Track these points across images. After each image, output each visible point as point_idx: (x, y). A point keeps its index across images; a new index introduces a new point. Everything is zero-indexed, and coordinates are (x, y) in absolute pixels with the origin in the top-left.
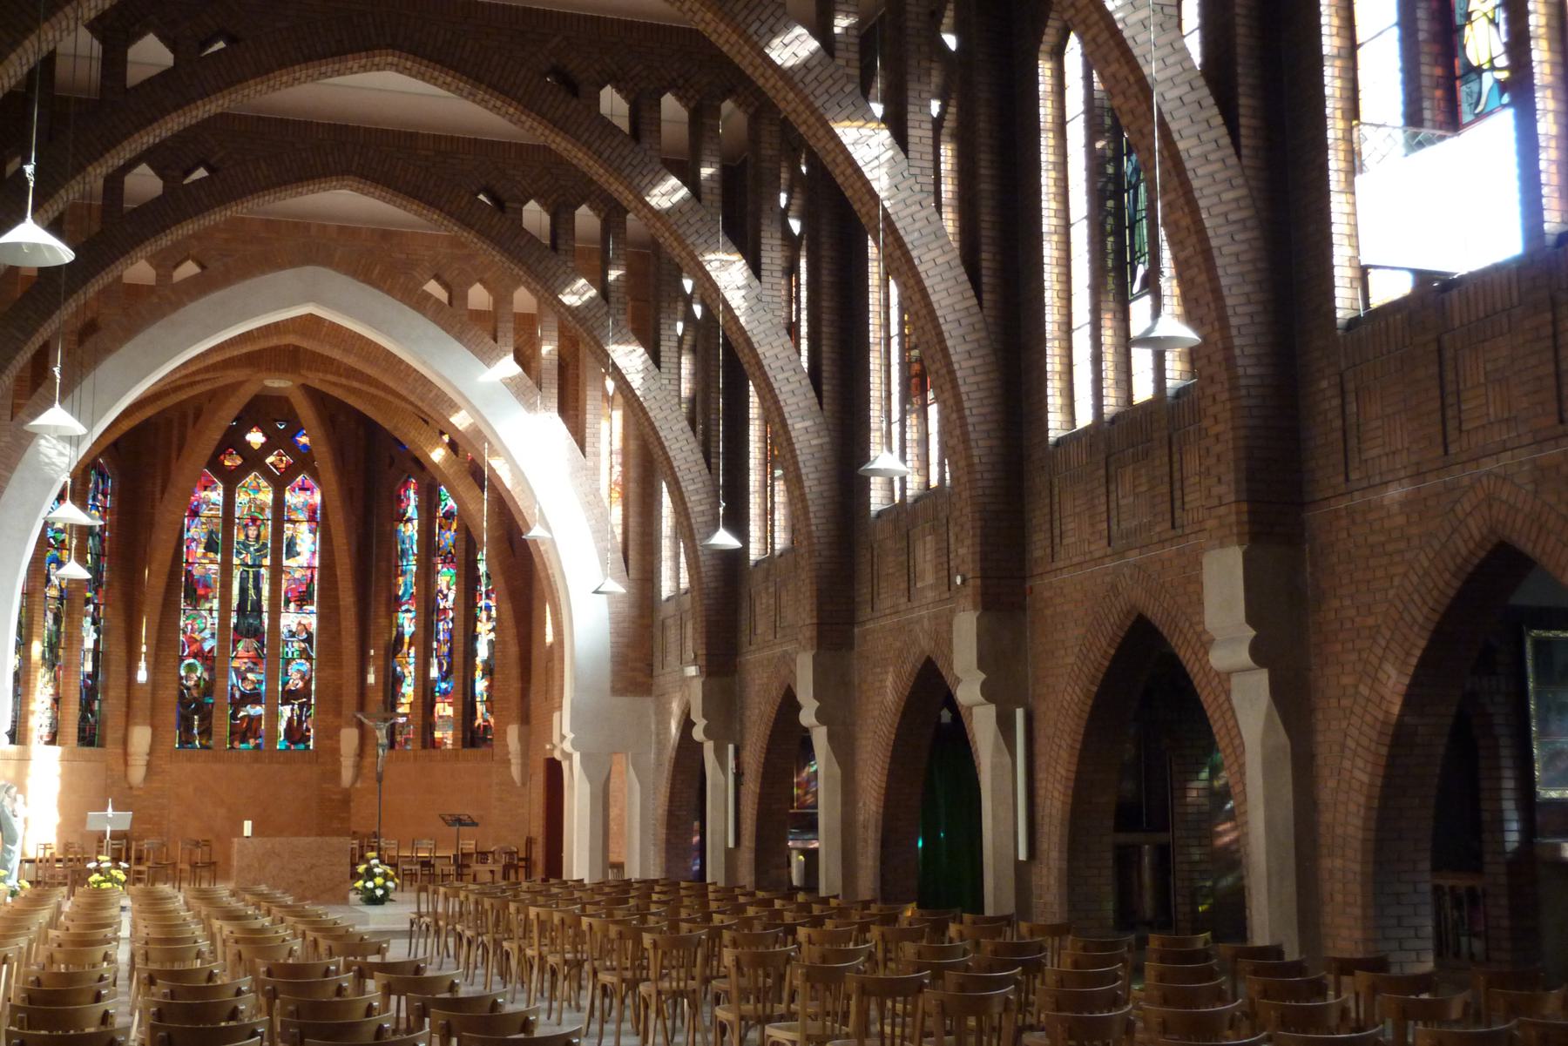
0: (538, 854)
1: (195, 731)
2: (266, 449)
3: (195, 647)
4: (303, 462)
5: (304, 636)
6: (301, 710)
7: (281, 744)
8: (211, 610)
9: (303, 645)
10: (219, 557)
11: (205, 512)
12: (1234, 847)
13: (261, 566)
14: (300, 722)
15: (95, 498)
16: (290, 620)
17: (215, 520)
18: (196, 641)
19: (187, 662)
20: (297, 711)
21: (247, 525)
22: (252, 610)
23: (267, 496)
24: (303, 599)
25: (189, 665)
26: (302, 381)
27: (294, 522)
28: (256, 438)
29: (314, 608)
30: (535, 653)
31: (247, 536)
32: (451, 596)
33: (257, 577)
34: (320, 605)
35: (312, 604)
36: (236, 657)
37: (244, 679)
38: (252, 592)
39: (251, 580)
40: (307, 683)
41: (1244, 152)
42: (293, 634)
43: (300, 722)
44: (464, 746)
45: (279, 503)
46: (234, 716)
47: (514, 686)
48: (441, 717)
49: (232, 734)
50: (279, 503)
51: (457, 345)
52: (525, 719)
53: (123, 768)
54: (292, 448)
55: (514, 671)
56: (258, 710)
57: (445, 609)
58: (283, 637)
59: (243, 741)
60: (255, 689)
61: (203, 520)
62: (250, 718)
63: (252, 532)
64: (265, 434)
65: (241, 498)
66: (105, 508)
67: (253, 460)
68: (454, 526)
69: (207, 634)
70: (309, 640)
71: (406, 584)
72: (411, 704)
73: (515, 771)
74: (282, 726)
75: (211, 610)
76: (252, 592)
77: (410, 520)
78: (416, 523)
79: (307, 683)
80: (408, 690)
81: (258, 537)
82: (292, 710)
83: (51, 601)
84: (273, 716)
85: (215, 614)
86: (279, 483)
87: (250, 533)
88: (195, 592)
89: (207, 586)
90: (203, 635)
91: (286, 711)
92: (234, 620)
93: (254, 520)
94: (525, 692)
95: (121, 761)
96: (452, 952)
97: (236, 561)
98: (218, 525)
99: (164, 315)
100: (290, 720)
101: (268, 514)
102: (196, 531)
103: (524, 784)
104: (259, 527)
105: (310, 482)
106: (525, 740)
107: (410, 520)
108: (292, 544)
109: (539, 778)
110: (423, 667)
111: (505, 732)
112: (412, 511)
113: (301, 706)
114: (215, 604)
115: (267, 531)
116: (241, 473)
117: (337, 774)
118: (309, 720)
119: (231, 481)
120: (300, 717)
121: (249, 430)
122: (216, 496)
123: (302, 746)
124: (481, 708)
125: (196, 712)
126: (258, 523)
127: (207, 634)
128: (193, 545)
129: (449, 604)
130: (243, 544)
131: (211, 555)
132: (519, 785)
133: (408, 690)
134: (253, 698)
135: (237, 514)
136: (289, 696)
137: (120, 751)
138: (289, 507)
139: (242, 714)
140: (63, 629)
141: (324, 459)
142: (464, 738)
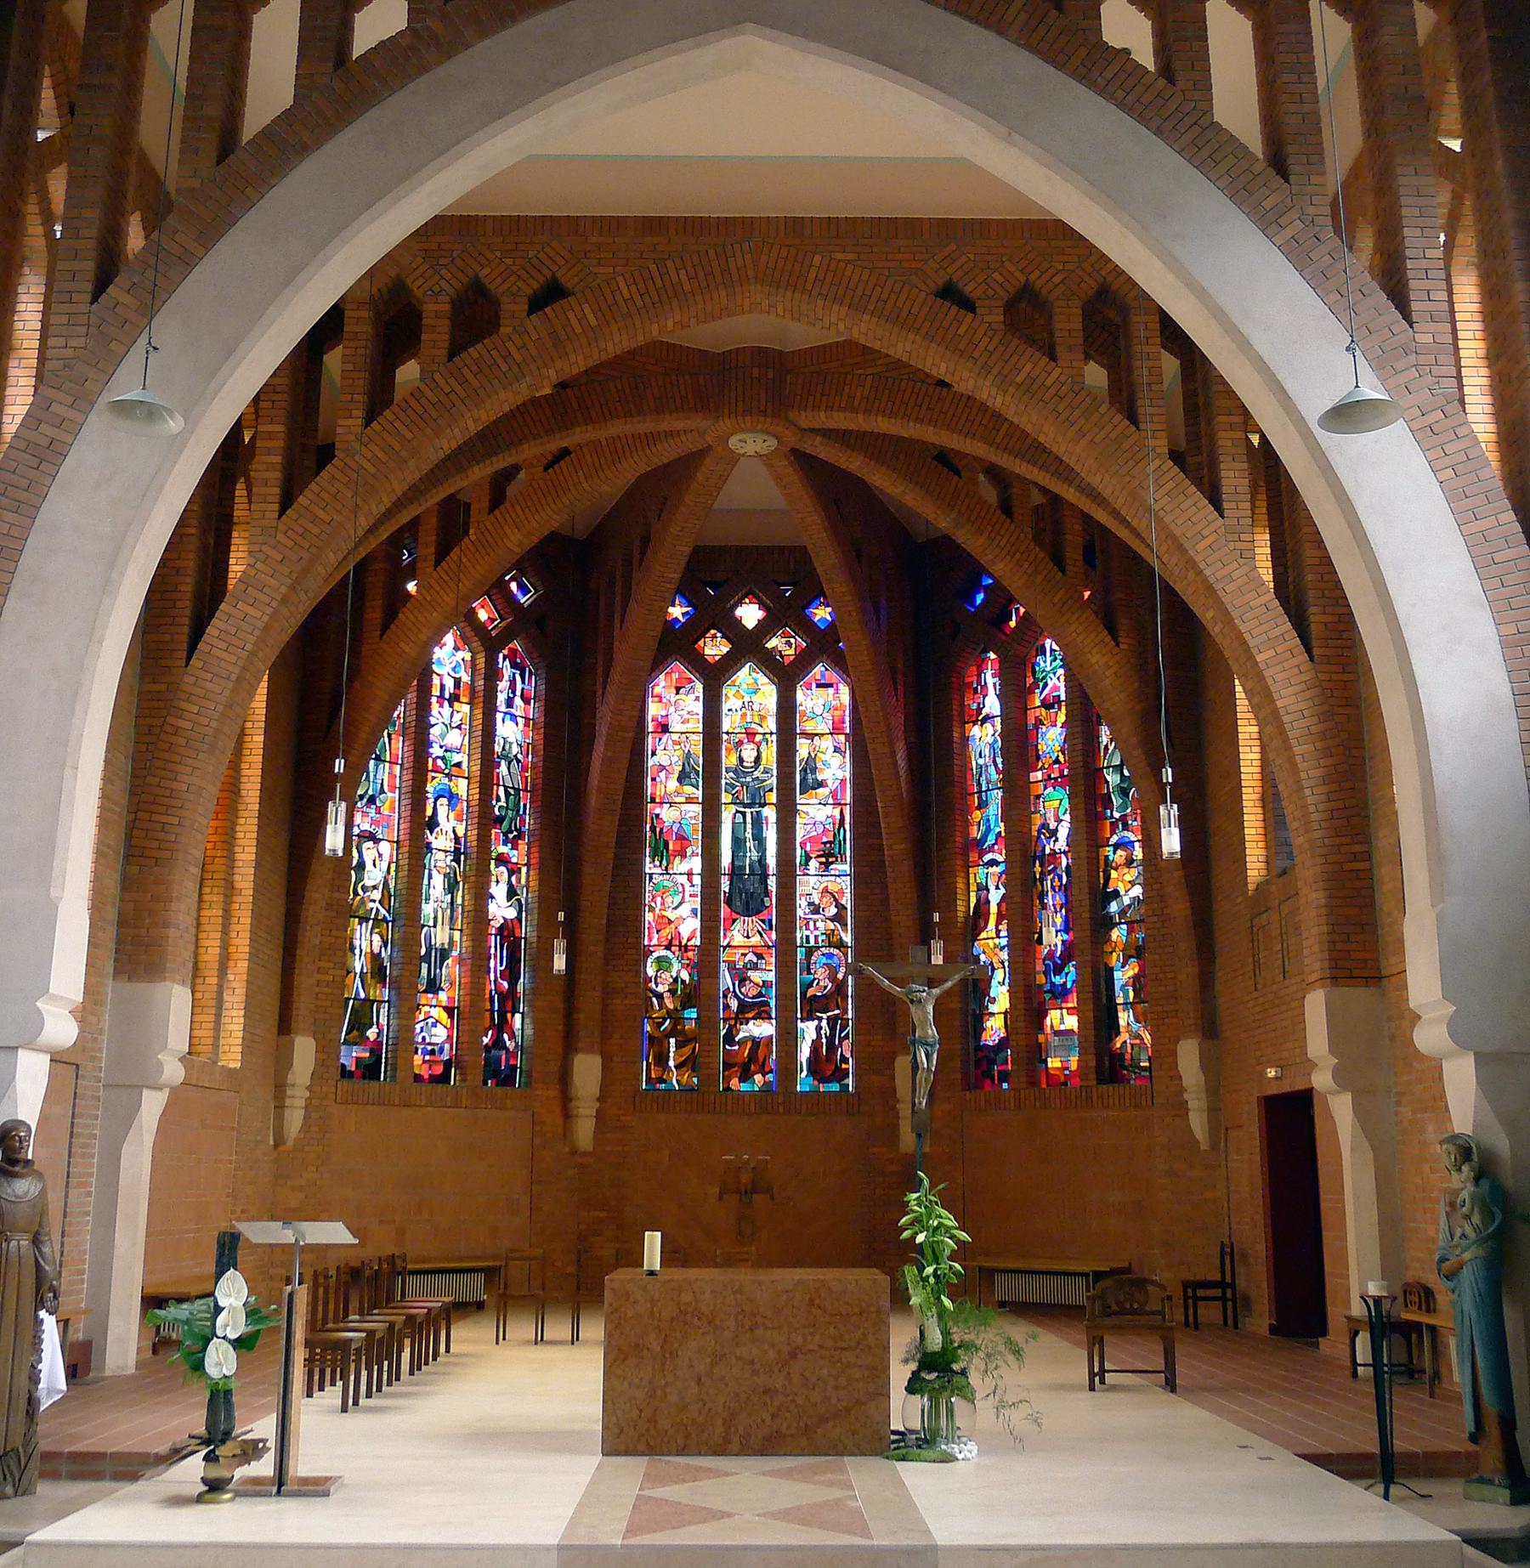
0: (1257, 1280)
1: (671, 1063)
2: (766, 628)
3: (667, 932)
4: (822, 645)
5: (833, 910)
6: (832, 1028)
7: (804, 1082)
8: (690, 874)
9: (831, 925)
10: (699, 794)
11: (676, 725)
12: (646, 1485)
13: (763, 805)
14: (832, 1047)
15: (510, 703)
16: (810, 885)
17: (693, 737)
18: (670, 922)
19: (655, 955)
20: (825, 1029)
21: (740, 743)
22: (752, 873)
23: (768, 696)
24: (829, 857)
25: (659, 960)
26: (792, 439)
27: (811, 736)
28: (750, 614)
29: (846, 868)
30: (1224, 908)
31: (741, 760)
32: (1063, 833)
33: (758, 822)
34: (855, 863)
35: (843, 861)
36: (728, 945)
37: (743, 980)
38: (750, 844)
39: (749, 826)
40: (840, 987)
41: (1316, 651)
42: (816, 909)
43: (832, 1047)
44: (1100, 1081)
45: (787, 710)
46: (729, 1038)
47: (1186, 973)
48: (1057, 1033)
49: (727, 1066)
50: (787, 710)
51: (1081, 91)
52: (1210, 1030)
53: (560, 1121)
54: (805, 626)
55: (1186, 946)
56: (763, 1029)
57: (1053, 853)
58: (800, 913)
59: (742, 1080)
60: (760, 995)
61: (675, 737)
62: (756, 1042)
63: (749, 753)
64: (762, 606)
65: (731, 701)
66: (527, 719)
67: (747, 647)
68: (1062, 718)
69: (685, 910)
70: (839, 918)
71: (989, 818)
72: (1005, 1013)
73: (1198, 1122)
74: (804, 1053)
75: (690, 874)
76: (750, 844)
77: (988, 718)
78: (998, 721)
79: (840, 987)
80: (1000, 997)
81: (758, 759)
82: (819, 1028)
83: (441, 855)
84: (788, 1036)
85: (697, 880)
86: (787, 677)
87: (745, 755)
88: (667, 848)
89: (682, 838)
90: (679, 912)
91: (808, 1030)
92: (725, 885)
93: (751, 735)
94: (1206, 981)
95: (558, 1110)
96: (433, 951)
97: (726, 798)
98: (696, 745)
99: (423, 69)
100: (816, 1045)
101: (771, 724)
102: (664, 756)
103: (1214, 1146)
104: (758, 745)
105: (833, 676)
106: (1211, 1065)
107: (988, 718)
108: (811, 765)
109: (1250, 1135)
110: (1025, 939)
111: (1174, 1053)
112: (992, 705)
113: (832, 1022)
114: (696, 864)
115: (770, 754)
116: (727, 666)
117: (891, 1134)
118: (847, 1044)
119: (715, 677)
120: (830, 1039)
121: (740, 603)
122: (693, 703)
123: (835, 1087)
124: (1124, 1018)
125: (671, 1033)
126: (758, 738)
127: (685, 910)
128: (663, 774)
129: (1062, 845)
130: (735, 771)
131: (688, 789)
132: (1204, 1146)
133: (1000, 997)
134: (755, 1009)
135: (726, 727)
136: (813, 1007)
137: (554, 1093)
138: (803, 714)
139: (741, 1035)
140: (459, 901)
141: (853, 642)
142: (1099, 1069)
